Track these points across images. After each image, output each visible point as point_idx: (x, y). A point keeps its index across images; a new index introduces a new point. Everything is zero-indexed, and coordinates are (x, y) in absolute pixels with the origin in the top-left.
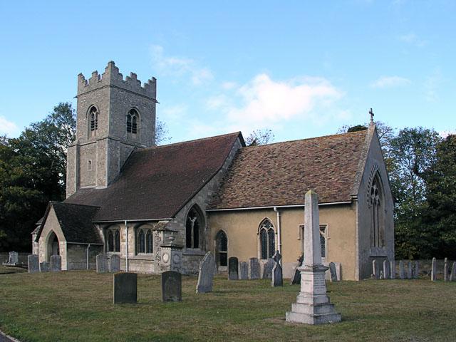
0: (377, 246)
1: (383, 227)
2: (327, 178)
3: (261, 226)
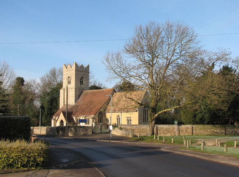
0: (147, 121)
3: (117, 117)
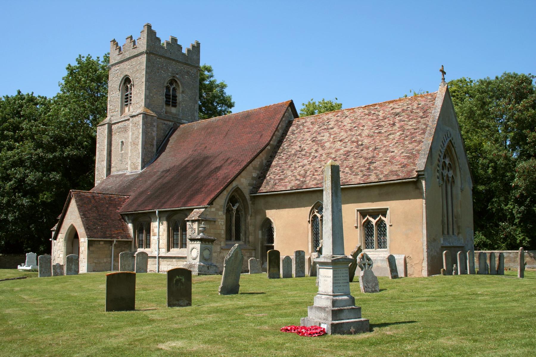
0: (451, 232)
1: (459, 210)
2: (388, 151)
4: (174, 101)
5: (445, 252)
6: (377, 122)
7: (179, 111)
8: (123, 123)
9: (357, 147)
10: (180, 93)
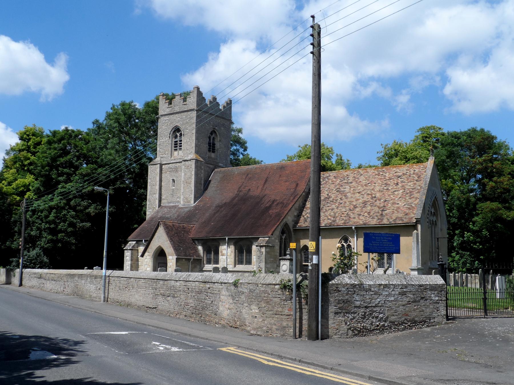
2: (394, 203)
4: (213, 148)
5: (434, 271)
6: (385, 181)
7: (217, 156)
8: (174, 164)
9: (372, 198)
10: (218, 142)
